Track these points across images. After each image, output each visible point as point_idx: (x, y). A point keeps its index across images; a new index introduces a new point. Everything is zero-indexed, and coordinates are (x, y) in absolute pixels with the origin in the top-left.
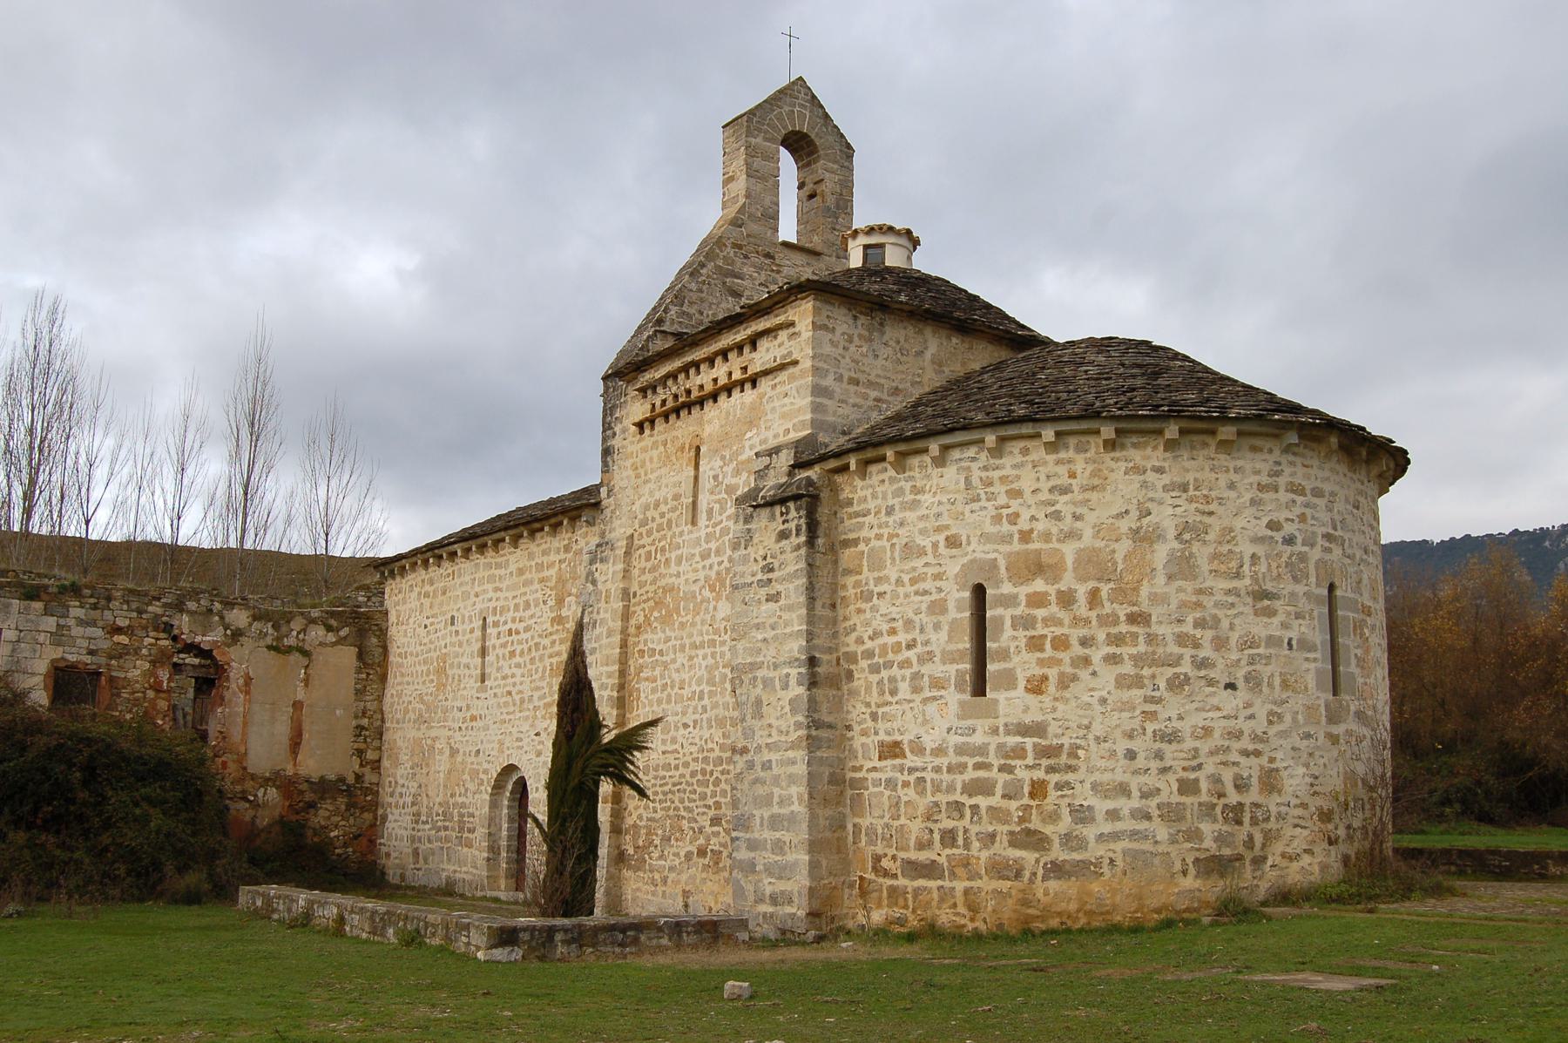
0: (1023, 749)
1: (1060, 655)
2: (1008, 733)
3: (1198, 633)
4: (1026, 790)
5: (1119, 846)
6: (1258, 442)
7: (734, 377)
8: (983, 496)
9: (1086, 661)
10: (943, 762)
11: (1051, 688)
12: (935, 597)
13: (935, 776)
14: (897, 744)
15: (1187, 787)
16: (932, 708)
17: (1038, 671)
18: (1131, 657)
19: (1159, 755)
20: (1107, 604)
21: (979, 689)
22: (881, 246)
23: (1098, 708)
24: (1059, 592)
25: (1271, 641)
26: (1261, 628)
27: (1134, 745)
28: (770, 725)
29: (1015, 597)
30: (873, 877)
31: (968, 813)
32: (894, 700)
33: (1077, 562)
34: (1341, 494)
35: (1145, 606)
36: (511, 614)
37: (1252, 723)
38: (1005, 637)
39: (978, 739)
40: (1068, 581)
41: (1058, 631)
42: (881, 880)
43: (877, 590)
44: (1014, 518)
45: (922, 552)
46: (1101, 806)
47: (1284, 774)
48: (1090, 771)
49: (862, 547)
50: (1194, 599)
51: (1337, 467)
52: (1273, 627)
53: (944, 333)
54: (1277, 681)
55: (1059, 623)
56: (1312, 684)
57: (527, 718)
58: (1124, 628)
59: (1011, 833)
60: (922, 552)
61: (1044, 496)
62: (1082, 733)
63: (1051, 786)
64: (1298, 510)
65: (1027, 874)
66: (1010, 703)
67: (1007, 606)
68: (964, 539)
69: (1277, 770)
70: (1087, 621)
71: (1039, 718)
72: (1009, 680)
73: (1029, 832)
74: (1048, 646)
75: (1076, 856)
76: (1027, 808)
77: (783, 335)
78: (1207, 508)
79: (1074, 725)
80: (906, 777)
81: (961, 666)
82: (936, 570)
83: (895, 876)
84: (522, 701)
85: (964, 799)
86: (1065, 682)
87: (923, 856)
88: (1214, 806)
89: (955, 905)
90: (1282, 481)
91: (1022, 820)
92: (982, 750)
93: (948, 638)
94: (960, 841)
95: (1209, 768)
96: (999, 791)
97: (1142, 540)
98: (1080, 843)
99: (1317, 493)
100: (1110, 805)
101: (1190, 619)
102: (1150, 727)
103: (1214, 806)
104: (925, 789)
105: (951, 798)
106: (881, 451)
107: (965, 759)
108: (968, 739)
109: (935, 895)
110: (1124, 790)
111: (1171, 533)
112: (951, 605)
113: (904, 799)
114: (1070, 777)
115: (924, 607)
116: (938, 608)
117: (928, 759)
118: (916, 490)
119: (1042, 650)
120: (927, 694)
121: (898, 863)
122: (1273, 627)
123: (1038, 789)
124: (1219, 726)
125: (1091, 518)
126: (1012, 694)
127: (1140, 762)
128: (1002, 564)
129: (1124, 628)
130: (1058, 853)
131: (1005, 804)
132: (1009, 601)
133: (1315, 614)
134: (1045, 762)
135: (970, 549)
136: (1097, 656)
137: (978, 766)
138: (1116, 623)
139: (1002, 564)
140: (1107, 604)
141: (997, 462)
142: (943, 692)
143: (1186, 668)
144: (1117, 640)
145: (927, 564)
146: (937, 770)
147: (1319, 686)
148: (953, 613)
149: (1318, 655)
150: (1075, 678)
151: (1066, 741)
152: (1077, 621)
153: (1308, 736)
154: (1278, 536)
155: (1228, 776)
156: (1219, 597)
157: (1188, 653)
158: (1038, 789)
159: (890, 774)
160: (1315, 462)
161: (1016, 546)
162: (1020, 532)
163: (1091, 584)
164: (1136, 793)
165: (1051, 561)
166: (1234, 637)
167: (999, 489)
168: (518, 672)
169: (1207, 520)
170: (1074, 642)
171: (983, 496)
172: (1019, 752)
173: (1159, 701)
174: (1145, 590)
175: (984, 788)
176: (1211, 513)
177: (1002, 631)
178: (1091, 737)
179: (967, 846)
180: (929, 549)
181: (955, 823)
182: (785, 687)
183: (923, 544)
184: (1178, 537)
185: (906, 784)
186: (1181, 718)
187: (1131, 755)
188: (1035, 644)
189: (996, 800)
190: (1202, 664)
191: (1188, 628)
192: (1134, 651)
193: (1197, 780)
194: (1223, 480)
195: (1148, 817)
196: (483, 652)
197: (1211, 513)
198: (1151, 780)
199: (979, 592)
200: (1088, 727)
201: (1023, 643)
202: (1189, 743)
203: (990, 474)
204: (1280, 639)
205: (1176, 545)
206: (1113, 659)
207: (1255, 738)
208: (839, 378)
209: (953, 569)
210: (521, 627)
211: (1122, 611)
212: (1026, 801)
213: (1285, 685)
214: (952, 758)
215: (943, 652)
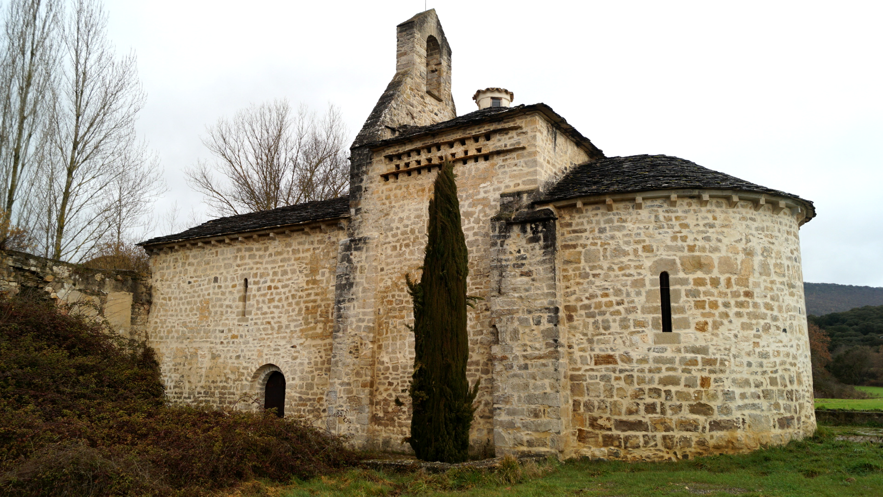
0: (696, 361)
1: (713, 311)
2: (687, 351)
4: (699, 382)
5: (746, 412)
7: (470, 154)
8: (666, 226)
9: (727, 315)
10: (646, 367)
12: (636, 277)
13: (640, 374)
14: (610, 356)
15: (773, 381)
16: (636, 338)
17: (702, 320)
18: (747, 313)
19: (761, 365)
20: (734, 286)
21: (667, 326)
24: (711, 278)
27: (750, 359)
28: (525, 345)
29: (687, 279)
30: (590, 429)
31: (663, 394)
32: (607, 332)
33: (720, 263)
35: (750, 289)
36: (271, 277)
38: (681, 301)
39: (668, 354)
41: (712, 299)
42: (597, 431)
43: (591, 272)
44: (684, 239)
45: (626, 254)
46: (738, 391)
48: (733, 372)
49: (579, 249)
55: (712, 295)
57: (284, 338)
58: (742, 298)
59: (691, 405)
60: (626, 254)
62: (727, 352)
63: (712, 380)
65: (701, 427)
66: (688, 336)
67: (682, 284)
68: (655, 248)
70: (726, 294)
71: (704, 344)
72: (685, 324)
74: (707, 306)
75: (725, 418)
76: (699, 392)
77: (513, 133)
78: (771, 241)
79: (722, 348)
80: (617, 374)
81: (655, 315)
82: (637, 264)
83: (610, 429)
84: (280, 328)
85: (660, 387)
86: (716, 325)
87: (632, 418)
88: (783, 392)
89: (656, 445)
91: (697, 398)
92: (671, 361)
93: (646, 299)
94: (658, 410)
95: (780, 373)
96: (683, 382)
98: (726, 410)
100: (742, 390)
102: (757, 350)
103: (783, 392)
104: (632, 381)
105: (652, 386)
106: (602, 198)
107: (661, 365)
108: (662, 355)
109: (642, 440)
110: (747, 383)
111: (759, 252)
112: (647, 282)
113: (616, 386)
114: (721, 375)
115: (629, 283)
117: (635, 365)
118: (622, 220)
119: (704, 308)
120: (632, 329)
121: (612, 422)
123: (705, 382)
125: (725, 241)
126: (687, 331)
127: (754, 368)
128: (678, 261)
129: (742, 298)
130: (717, 417)
131: (686, 390)
132: (684, 282)
134: (708, 368)
135: (659, 253)
137: (668, 369)
138: (739, 296)
139: (678, 261)
140: (734, 286)
141: (674, 209)
142: (644, 329)
143: (768, 321)
145: (630, 260)
146: (642, 371)
148: (648, 287)
150: (722, 324)
151: (718, 356)
152: (721, 294)
156: (778, 285)
157: (769, 312)
158: (705, 382)
159: (604, 373)
161: (686, 253)
162: (688, 246)
163: (727, 275)
164: (753, 385)
165: (706, 262)
168: (276, 311)
171: (666, 226)
172: (694, 362)
173: (759, 337)
175: (675, 381)
176: (773, 243)
177: (680, 297)
178: (731, 355)
179: (663, 412)
180: (631, 252)
181: (655, 400)
182: (538, 323)
183: (627, 249)
184: (762, 254)
185: (617, 379)
187: (749, 364)
188: (700, 305)
189: (681, 388)
191: (768, 300)
192: (748, 310)
195: (759, 397)
196: (244, 299)
197: (773, 243)
198: (759, 378)
199: (664, 278)
200: (729, 350)
201: (693, 304)
203: (670, 214)
206: (739, 315)
209: (648, 263)
210: (279, 285)
211: (742, 290)
212: (699, 388)
214: (652, 365)
215: (643, 308)
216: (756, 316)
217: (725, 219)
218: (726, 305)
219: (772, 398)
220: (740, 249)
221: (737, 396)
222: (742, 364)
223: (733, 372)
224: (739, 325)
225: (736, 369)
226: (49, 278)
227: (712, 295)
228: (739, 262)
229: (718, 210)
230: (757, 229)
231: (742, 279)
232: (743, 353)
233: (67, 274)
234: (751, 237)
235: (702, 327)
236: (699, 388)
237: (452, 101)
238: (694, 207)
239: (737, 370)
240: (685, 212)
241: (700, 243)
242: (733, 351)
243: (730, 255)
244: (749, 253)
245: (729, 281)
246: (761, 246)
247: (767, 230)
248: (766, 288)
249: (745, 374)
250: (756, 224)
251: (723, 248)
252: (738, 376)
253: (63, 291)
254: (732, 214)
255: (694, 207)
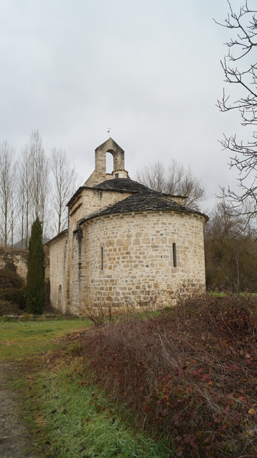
1: (114, 261)
2: (106, 277)
3: (140, 255)
6: (154, 214)
9: (118, 262)
11: (112, 268)
15: (138, 288)
17: (110, 265)
18: (127, 261)
19: (132, 281)
22: (118, 174)
23: (121, 272)
25: (157, 256)
26: (154, 254)
27: (127, 279)
33: (117, 242)
34: (178, 223)
37: (152, 274)
39: (102, 279)
40: (115, 246)
41: (114, 256)
46: (121, 292)
47: (160, 284)
48: (120, 284)
50: (139, 248)
51: (177, 218)
52: (157, 253)
53: (116, 193)
54: (158, 265)
55: (113, 255)
56: (167, 265)
58: (125, 255)
61: (111, 229)
64: (164, 228)
66: (107, 271)
69: (158, 283)
70: (119, 254)
71: (110, 274)
73: (109, 297)
76: (109, 293)
78: (142, 229)
86: (114, 267)
90: (160, 222)
92: (102, 281)
95: (142, 284)
97: (129, 237)
99: (170, 224)
100: (123, 291)
101: (138, 253)
102: (130, 275)
112: (98, 252)
114: (116, 286)
116: (96, 252)
122: (157, 253)
123: (110, 289)
124: (145, 274)
125: (119, 233)
127: (128, 283)
128: (105, 243)
129: (125, 255)
133: (169, 250)
134: (112, 283)
136: (120, 261)
138: (124, 254)
139: (105, 243)
143: (137, 263)
144: (124, 258)
147: (170, 265)
149: (169, 258)
150: (117, 266)
151: (115, 279)
153: (167, 276)
154: (159, 234)
155: (146, 285)
156: (144, 248)
157: (138, 260)
158: (110, 289)
160: (169, 217)
161: (107, 240)
163: (119, 247)
164: (127, 289)
166: (148, 256)
167: (104, 228)
169: (142, 232)
170: (116, 258)
172: (107, 281)
173: (132, 270)
174: (129, 247)
176: (143, 230)
184: (136, 236)
186: (136, 273)
187: (126, 281)
188: (110, 259)
190: (141, 262)
191: (138, 255)
192: (127, 260)
193: (140, 286)
194: (146, 223)
195: (130, 294)
197: (143, 230)
198: (131, 286)
202: (138, 278)
204: (159, 256)
205: (136, 238)
207: (153, 277)
208: (90, 206)
209: (98, 245)
211: (125, 252)
213: (160, 265)
216: (131, 262)
217: (120, 224)
218: (118, 258)
219: (136, 294)
220: (125, 235)
221: (121, 294)
222: (123, 281)
223: (120, 284)
224: (123, 266)
225: (121, 283)
226: (14, 260)
227: (113, 255)
228: (124, 241)
229: (117, 221)
230: (134, 226)
231: (125, 247)
232: (124, 277)
233: (20, 258)
234: (131, 230)
235: (110, 268)
236: (109, 291)
237: (87, 181)
238: (110, 221)
239: (121, 283)
240: (107, 223)
241: (111, 235)
242: (120, 276)
243: (121, 238)
244: (129, 236)
245: (120, 249)
246: (136, 232)
247: (140, 225)
248: (137, 250)
249: (124, 285)
250: (133, 224)
251: (118, 235)
252: (121, 286)
253: (19, 263)
254: (122, 222)
255: (110, 221)
